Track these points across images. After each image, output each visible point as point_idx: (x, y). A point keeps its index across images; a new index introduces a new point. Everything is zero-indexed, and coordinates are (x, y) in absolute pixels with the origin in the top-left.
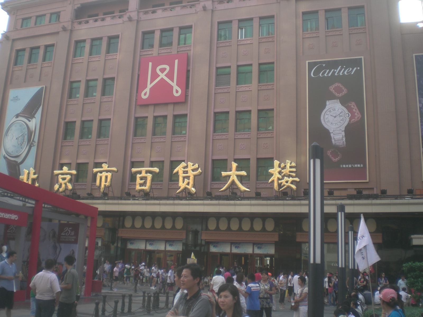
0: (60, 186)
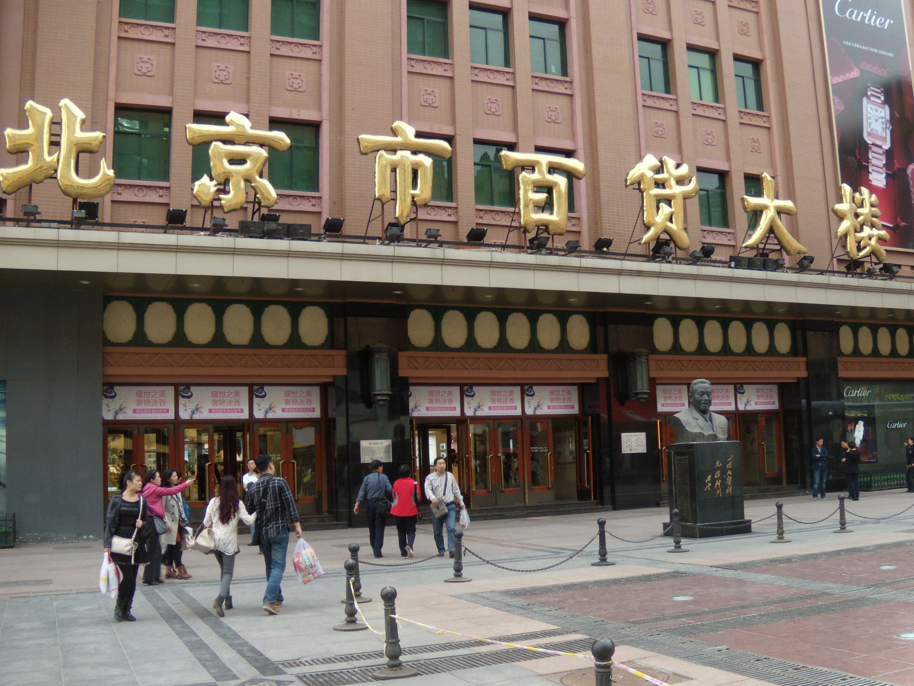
0: (223, 188)
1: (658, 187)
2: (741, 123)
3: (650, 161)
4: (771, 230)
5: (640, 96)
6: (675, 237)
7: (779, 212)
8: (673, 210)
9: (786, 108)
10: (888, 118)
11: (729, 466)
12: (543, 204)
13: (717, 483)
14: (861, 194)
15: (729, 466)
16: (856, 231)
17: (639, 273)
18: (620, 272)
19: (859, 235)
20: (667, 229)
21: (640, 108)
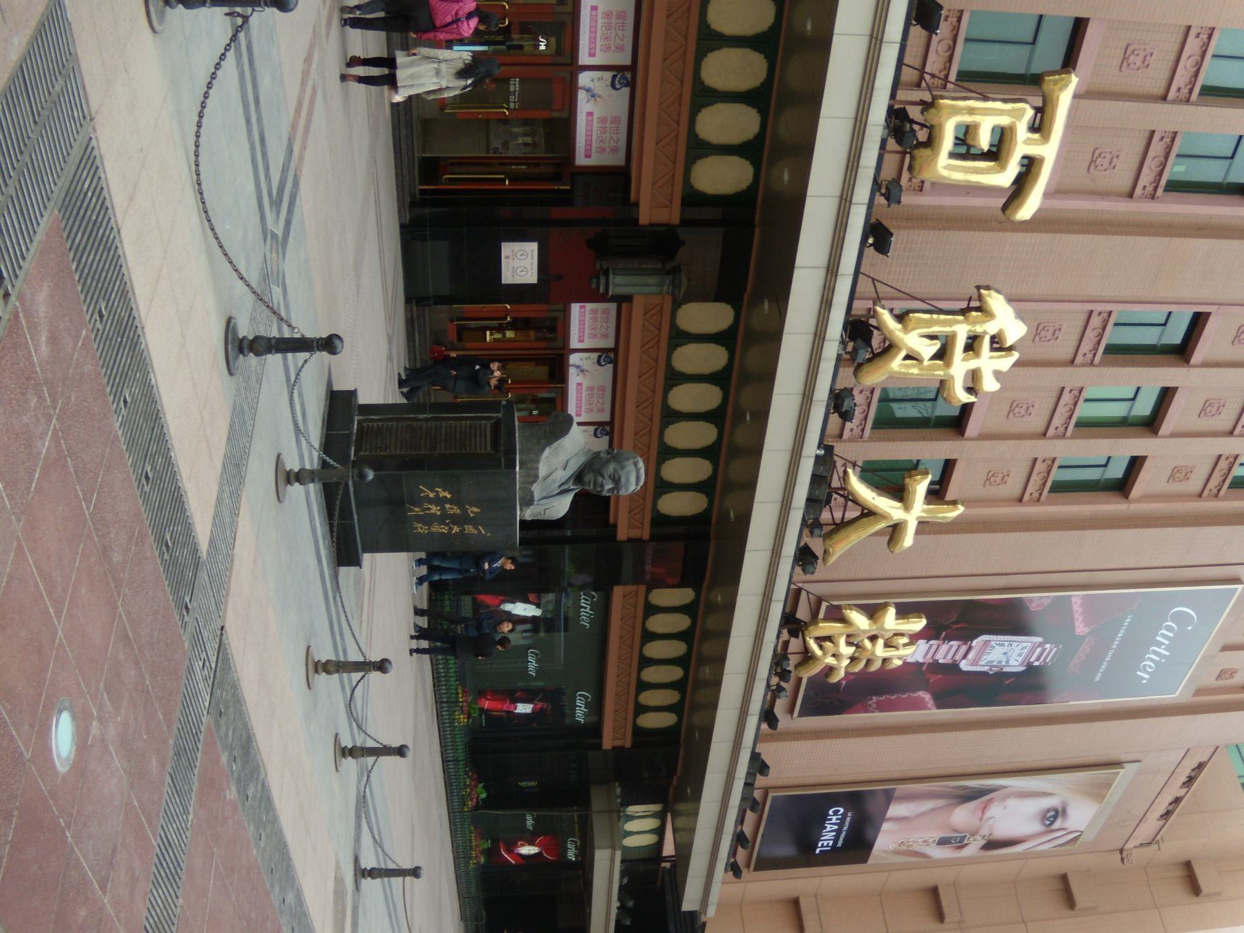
1: (969, 338)
2: (1036, 459)
3: (1015, 330)
4: (868, 513)
5: (1108, 307)
6: (878, 363)
7: (896, 529)
8: (926, 363)
9: (1047, 529)
10: (1006, 670)
11: (470, 529)
12: (969, 141)
13: (434, 501)
14: (905, 645)
15: (470, 529)
16: (848, 636)
17: (826, 303)
18: (832, 269)
19: (842, 640)
20: (894, 350)
21: (1090, 307)
